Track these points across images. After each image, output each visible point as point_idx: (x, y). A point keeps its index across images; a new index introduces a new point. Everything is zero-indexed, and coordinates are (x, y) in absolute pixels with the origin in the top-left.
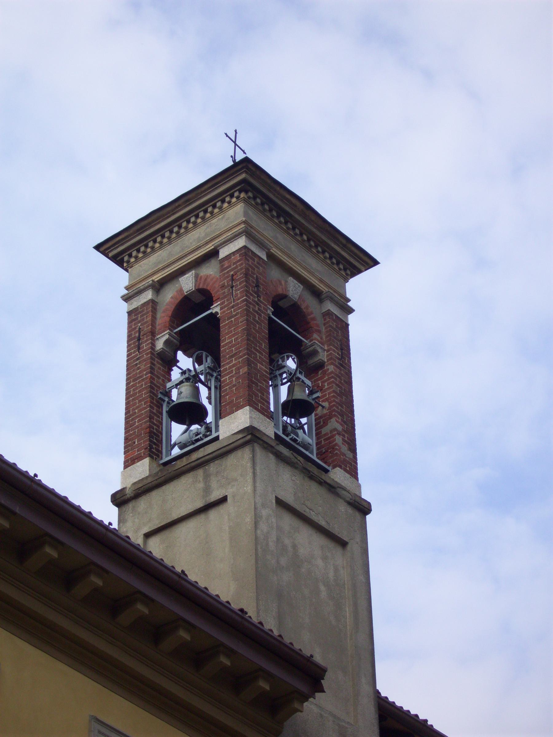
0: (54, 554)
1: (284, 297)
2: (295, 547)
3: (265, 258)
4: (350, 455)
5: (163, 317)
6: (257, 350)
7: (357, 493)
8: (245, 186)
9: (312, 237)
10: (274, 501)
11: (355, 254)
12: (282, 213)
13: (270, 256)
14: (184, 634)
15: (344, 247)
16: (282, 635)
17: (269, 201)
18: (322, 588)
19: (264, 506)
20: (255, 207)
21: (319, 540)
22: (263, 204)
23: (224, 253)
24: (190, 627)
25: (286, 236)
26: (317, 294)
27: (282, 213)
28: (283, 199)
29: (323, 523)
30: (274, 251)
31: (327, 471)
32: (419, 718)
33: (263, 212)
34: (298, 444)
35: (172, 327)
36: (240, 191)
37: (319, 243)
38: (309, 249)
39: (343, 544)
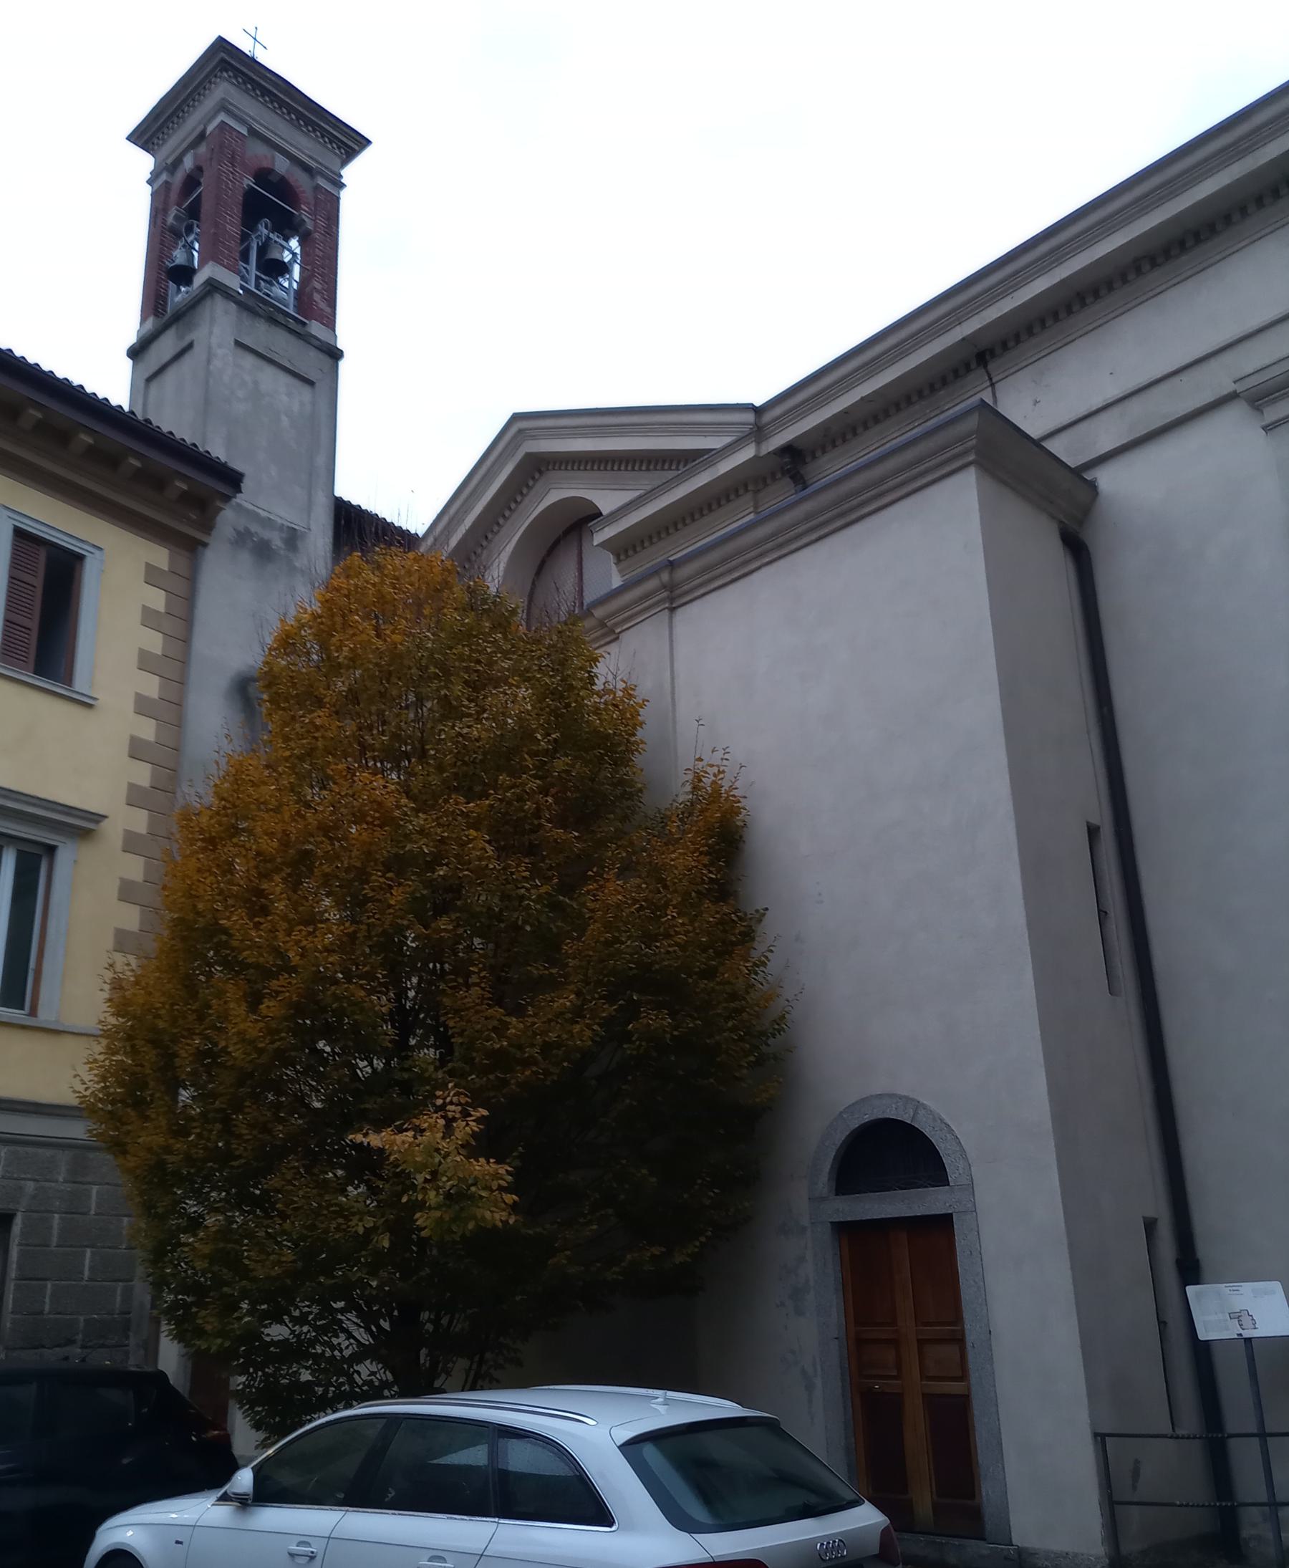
0: (39, 415)
1: (270, 171)
2: (256, 383)
3: (245, 133)
4: (328, 310)
5: (174, 196)
6: (227, 214)
7: (333, 343)
8: (224, 66)
9: (300, 116)
10: (233, 343)
11: (346, 133)
12: (265, 92)
13: (253, 132)
14: (87, 439)
15: (335, 127)
16: (134, 410)
17: (252, 81)
18: (284, 418)
19: (220, 346)
20: (237, 87)
21: (284, 379)
22: (245, 83)
23: (210, 129)
24: (185, 478)
25: (273, 115)
26: (307, 169)
27: (265, 92)
28: (264, 78)
29: (288, 365)
30: (256, 126)
31: (304, 324)
32: (404, 539)
33: (246, 91)
34: (272, 298)
35: (179, 205)
36: (221, 71)
37: (308, 122)
38: (299, 127)
39: (311, 383)
